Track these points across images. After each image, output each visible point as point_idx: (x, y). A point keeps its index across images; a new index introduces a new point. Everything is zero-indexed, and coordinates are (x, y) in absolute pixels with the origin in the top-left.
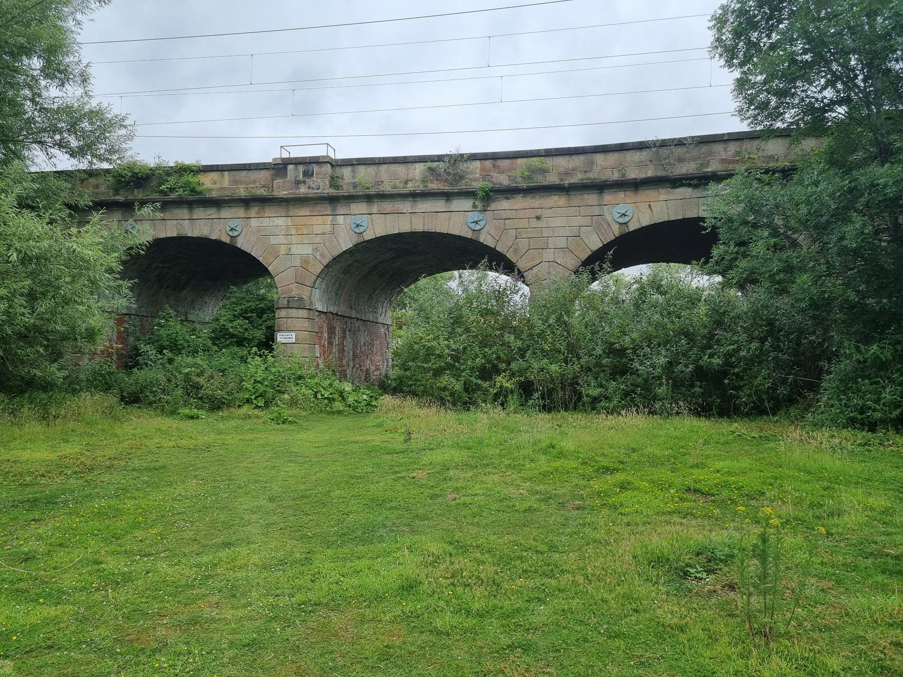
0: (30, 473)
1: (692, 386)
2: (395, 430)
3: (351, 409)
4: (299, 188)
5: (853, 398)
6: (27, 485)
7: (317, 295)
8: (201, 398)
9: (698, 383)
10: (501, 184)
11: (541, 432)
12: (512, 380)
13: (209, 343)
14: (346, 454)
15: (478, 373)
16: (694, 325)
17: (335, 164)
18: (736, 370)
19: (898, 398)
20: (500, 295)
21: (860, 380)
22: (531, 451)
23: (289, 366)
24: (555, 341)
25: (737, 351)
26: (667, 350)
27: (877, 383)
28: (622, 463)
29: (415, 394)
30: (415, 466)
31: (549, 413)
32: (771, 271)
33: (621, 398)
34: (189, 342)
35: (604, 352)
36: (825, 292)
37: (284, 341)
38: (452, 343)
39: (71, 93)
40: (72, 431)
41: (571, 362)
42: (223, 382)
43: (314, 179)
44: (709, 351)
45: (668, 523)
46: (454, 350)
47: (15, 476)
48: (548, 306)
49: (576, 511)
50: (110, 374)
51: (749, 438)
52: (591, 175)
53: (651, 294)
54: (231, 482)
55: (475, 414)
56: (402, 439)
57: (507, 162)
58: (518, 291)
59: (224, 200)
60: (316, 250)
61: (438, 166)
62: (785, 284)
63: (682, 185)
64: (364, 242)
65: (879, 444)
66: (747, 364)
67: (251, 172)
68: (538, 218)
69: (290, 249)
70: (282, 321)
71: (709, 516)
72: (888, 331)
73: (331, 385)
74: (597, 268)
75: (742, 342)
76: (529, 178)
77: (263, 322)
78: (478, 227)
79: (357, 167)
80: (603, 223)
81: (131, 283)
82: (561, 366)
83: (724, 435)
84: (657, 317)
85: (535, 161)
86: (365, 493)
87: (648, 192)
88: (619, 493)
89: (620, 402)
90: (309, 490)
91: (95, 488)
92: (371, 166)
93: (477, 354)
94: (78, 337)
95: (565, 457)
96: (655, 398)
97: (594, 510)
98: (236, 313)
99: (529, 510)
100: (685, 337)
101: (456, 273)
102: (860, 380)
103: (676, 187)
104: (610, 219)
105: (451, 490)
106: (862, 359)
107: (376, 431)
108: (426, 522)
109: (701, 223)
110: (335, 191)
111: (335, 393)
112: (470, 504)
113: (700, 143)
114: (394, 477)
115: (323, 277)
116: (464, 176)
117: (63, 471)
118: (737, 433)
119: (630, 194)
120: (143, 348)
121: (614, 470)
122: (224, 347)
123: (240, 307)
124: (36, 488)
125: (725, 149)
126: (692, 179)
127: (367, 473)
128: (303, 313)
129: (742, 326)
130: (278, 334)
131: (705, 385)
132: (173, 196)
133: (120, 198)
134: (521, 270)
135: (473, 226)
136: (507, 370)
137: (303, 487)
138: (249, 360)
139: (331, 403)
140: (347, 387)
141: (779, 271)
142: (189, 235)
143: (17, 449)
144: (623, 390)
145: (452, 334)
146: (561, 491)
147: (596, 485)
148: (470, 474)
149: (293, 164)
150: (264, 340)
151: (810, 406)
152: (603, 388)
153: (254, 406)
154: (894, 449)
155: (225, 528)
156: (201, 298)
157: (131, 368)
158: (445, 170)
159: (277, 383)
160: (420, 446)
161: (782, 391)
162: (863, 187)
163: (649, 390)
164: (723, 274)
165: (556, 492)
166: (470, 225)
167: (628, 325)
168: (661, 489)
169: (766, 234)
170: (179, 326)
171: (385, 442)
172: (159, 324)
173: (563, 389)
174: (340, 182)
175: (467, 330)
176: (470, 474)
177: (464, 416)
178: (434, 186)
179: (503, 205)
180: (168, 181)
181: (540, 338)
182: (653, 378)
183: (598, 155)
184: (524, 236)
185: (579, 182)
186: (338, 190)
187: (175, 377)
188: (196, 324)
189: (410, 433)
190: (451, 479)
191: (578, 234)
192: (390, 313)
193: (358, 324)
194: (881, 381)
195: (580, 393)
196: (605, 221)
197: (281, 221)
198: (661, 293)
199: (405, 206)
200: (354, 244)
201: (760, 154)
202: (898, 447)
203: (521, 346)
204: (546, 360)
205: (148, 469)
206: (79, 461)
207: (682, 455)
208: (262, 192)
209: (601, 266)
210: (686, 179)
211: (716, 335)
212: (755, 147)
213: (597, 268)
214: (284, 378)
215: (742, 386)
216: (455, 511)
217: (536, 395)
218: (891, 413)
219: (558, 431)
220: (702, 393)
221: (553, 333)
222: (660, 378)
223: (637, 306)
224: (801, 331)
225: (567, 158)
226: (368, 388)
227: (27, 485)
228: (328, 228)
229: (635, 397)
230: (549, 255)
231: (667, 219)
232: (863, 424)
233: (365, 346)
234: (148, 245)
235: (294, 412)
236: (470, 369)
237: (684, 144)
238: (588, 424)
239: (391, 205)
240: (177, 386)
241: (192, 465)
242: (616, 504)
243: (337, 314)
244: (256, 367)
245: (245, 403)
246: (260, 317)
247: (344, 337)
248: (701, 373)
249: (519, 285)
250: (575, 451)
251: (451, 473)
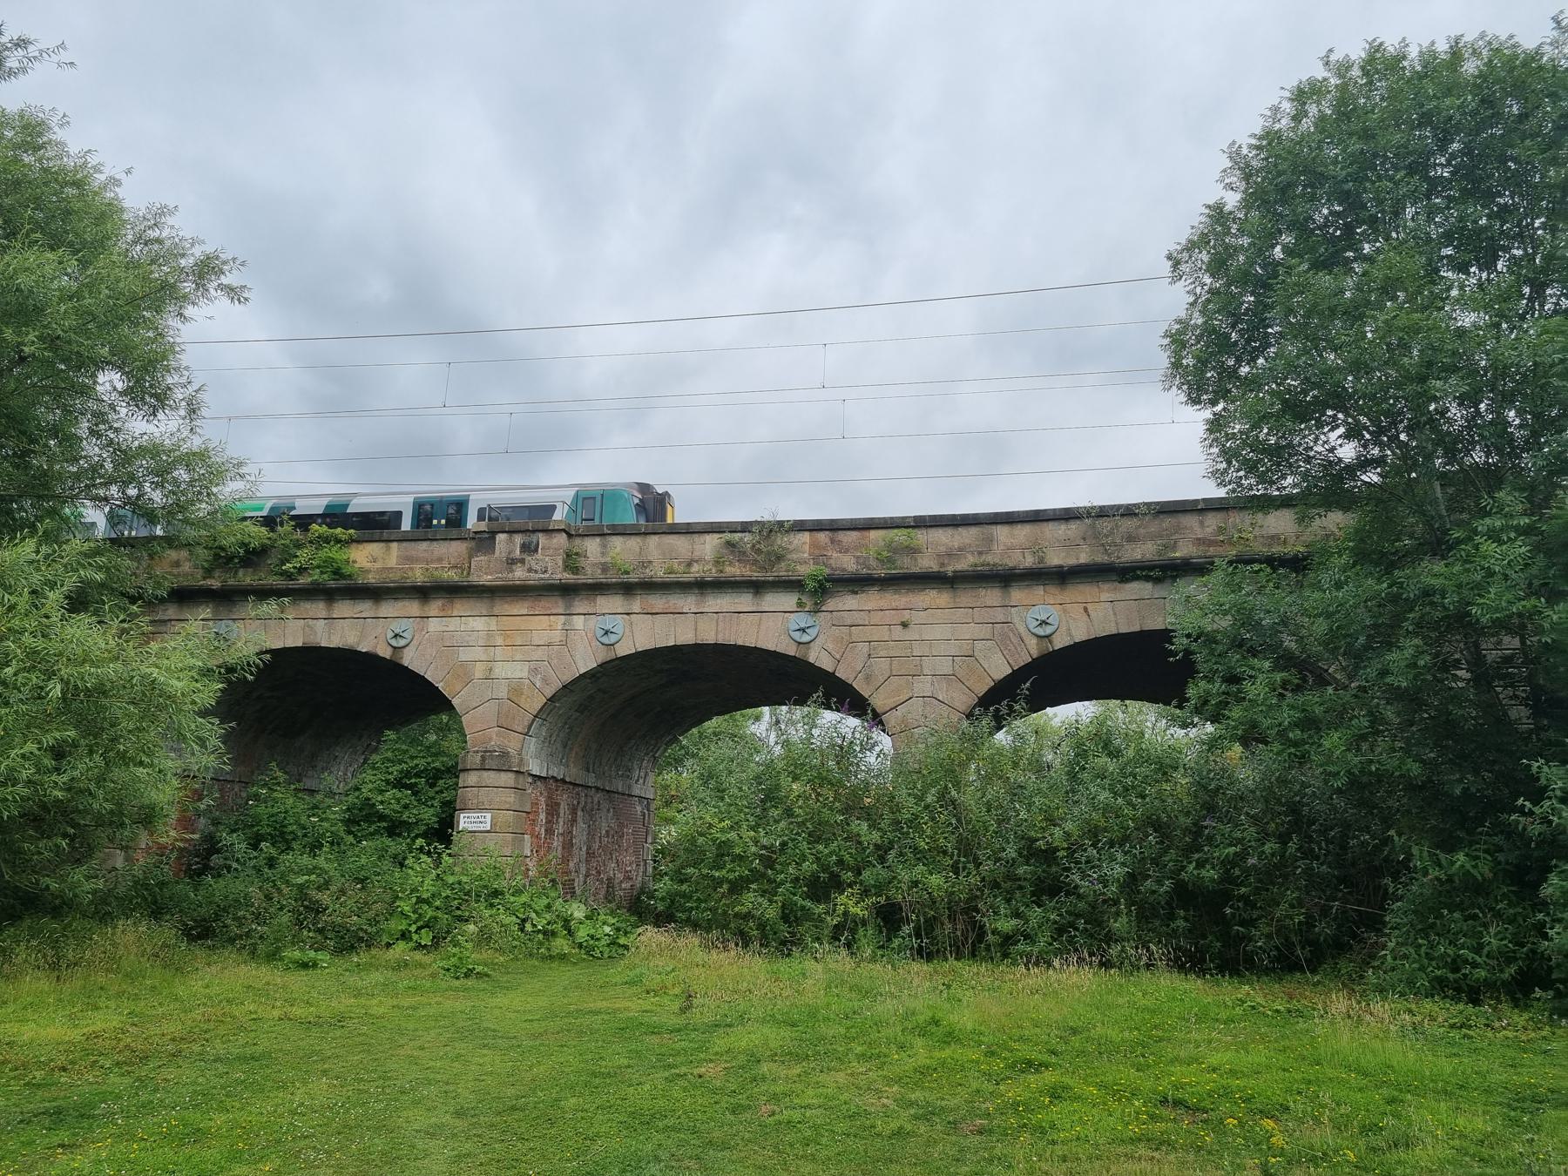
0: (40, 1065)
1: (1172, 917)
2: (662, 990)
3: (583, 952)
4: (512, 571)
6: (38, 1086)
8: (321, 931)
9: (1182, 913)
10: (844, 570)
12: (864, 901)
13: (341, 828)
14: (581, 1033)
15: (805, 889)
16: (1169, 809)
19: (1510, 945)
20: (844, 753)
21: (1446, 912)
22: (899, 1029)
23: (478, 873)
24: (936, 833)
25: (1242, 856)
26: (1126, 853)
27: (1475, 917)
28: (1054, 1053)
29: (695, 926)
30: (702, 1056)
31: (928, 962)
32: (1280, 725)
33: (1052, 937)
34: (304, 828)
35: (1020, 854)
36: (1371, 761)
38: (762, 834)
40: (101, 988)
42: (361, 901)
43: (539, 555)
44: (1196, 856)
45: (1129, 1157)
46: (764, 847)
47: (16, 1070)
48: (925, 772)
49: (978, 1137)
50: (162, 884)
51: (1269, 1013)
52: (989, 559)
53: (1094, 755)
55: (800, 963)
56: (676, 1006)
57: (854, 534)
58: (873, 746)
59: (388, 588)
60: (535, 671)
61: (741, 539)
62: (1307, 747)
63: (1137, 578)
66: (1260, 881)
67: (435, 543)
68: (905, 625)
69: (491, 670)
70: (470, 793)
71: (1198, 1146)
72: (1481, 829)
73: (548, 907)
74: (1004, 711)
75: (1249, 841)
76: (890, 560)
77: (437, 793)
78: (806, 638)
81: (224, 729)
82: (947, 877)
83: (1226, 1006)
84: (1104, 796)
85: (899, 536)
87: (1081, 587)
88: (1048, 1106)
89: (1051, 944)
90: (523, 1097)
91: (156, 1090)
92: (633, 537)
94: (127, 821)
96: (1110, 938)
97: (1007, 1135)
98: (390, 777)
99: (899, 1133)
100: (1155, 831)
102: (1446, 912)
104: (1022, 629)
105: (765, 1098)
106: (1443, 877)
107: (630, 992)
108: (727, 1153)
109: (1167, 645)
110: (572, 576)
112: (799, 1122)
115: (544, 717)
118: (1249, 1003)
120: (226, 838)
121: (1040, 1065)
122: (365, 837)
123: (398, 767)
124: (54, 1092)
125: (1202, 523)
126: (1152, 568)
127: (620, 1067)
128: (507, 779)
129: (1247, 814)
131: (1194, 916)
132: (304, 580)
133: (215, 583)
135: (797, 636)
136: (855, 883)
137: (511, 1091)
138: (410, 862)
139: (548, 940)
143: (11, 1022)
144: (1055, 922)
146: (953, 1102)
147: (1012, 1091)
148: (797, 1070)
149: (506, 532)
150: (436, 826)
151: (1373, 956)
153: (411, 944)
154: (1510, 1034)
155: (386, 1163)
157: (200, 873)
158: (754, 546)
159: (456, 902)
161: (1324, 929)
162: (1412, 596)
163: (1100, 924)
164: (1215, 719)
165: (944, 1103)
166: (792, 634)
167: (1058, 808)
168: (1119, 1100)
169: (1267, 664)
170: (291, 801)
171: (646, 1011)
172: (256, 797)
174: (582, 562)
175: (789, 813)
176: (797, 1070)
177: (783, 965)
178: (734, 571)
179: (847, 603)
180: (297, 556)
182: (1105, 901)
183: (999, 527)
184: (882, 653)
185: (970, 569)
186: (577, 574)
187: (279, 891)
188: (319, 797)
189: (690, 996)
191: (970, 653)
192: (651, 777)
193: (598, 796)
194: (1481, 915)
195: (982, 927)
197: (479, 624)
198: (1110, 755)
199: (688, 602)
200: (600, 662)
201: (1257, 532)
202: (1517, 1031)
203: (879, 842)
204: (921, 867)
205: (242, 1059)
206: (122, 1044)
207: (1156, 1041)
208: (451, 576)
209: (1010, 707)
210: (1142, 568)
211: (1206, 828)
212: (1248, 522)
213: (1004, 711)
214: (468, 893)
215: (1256, 920)
216: (774, 1134)
217: (906, 929)
218: (1502, 971)
221: (933, 819)
222: (1116, 902)
223: (1072, 776)
224: (1346, 826)
225: (950, 531)
226: (612, 913)
227: (38, 1086)
228: (557, 636)
230: (923, 686)
232: (1458, 990)
233: (608, 836)
235: (485, 955)
236: (791, 882)
237: (1136, 515)
238: (997, 983)
239: (664, 600)
242: (1044, 1124)
243: (563, 781)
244: (421, 874)
245: (397, 939)
247: (574, 821)
248: (1184, 894)
249: (874, 735)
250: (973, 1032)
251: (765, 1068)
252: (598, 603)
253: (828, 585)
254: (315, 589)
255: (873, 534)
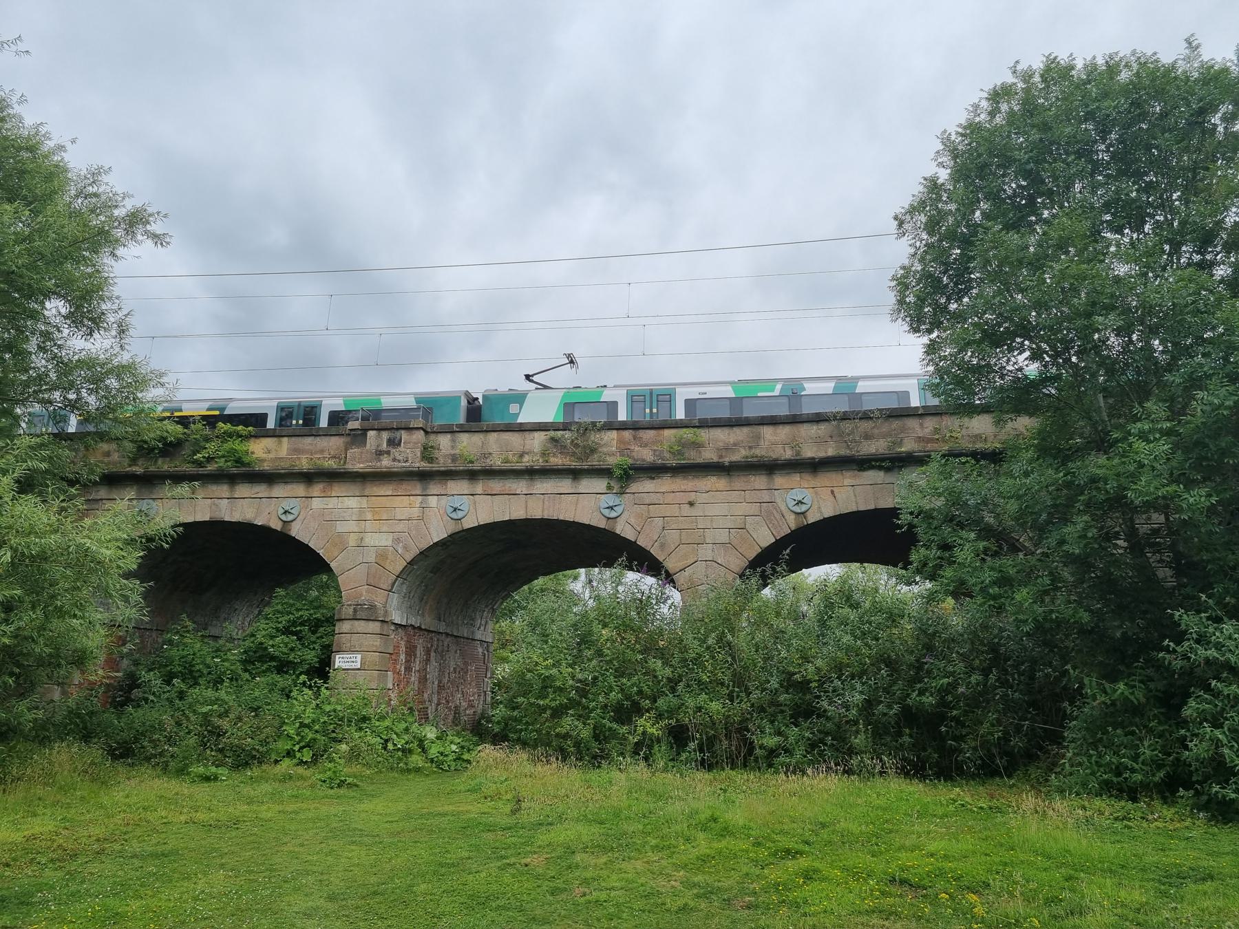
1: (900, 734)
2: (496, 797)
5: (1105, 753)
7: (395, 602)
8: (221, 751)
10: (644, 460)
11: (699, 800)
12: (658, 723)
13: (239, 667)
15: (612, 714)
17: (429, 430)
18: (955, 712)
19: (1160, 755)
20: (643, 604)
22: (685, 825)
23: (350, 702)
24: (716, 669)
25: (953, 686)
26: (863, 684)
27: (1133, 733)
28: (807, 843)
29: (524, 744)
30: (528, 849)
31: (709, 771)
32: (982, 582)
33: (806, 751)
35: (782, 686)
36: (1052, 611)
37: (345, 666)
38: (578, 671)
39: (99, 345)
40: (40, 799)
41: (737, 698)
42: (255, 726)
43: (402, 448)
44: (918, 686)
46: (580, 681)
48: (706, 620)
49: (747, 911)
50: (91, 714)
51: (975, 809)
52: (758, 452)
53: (839, 607)
54: (274, 874)
56: (508, 809)
57: (652, 433)
59: (280, 474)
60: (398, 540)
61: (563, 436)
63: (872, 468)
64: (463, 531)
65: (1141, 818)
66: (967, 705)
67: (318, 438)
68: (691, 504)
70: (344, 638)
73: (407, 730)
74: (769, 572)
75: (959, 674)
76: (680, 453)
77: (318, 638)
78: (613, 514)
79: (457, 435)
80: (775, 512)
83: (942, 805)
84: (847, 639)
86: (461, 887)
87: (828, 474)
88: (802, 886)
89: (805, 756)
91: (83, 882)
92: (476, 434)
93: (611, 687)
94: (63, 662)
95: (732, 834)
96: (851, 752)
99: (684, 909)
101: (582, 571)
102: (1110, 729)
103: (865, 470)
104: (783, 508)
105: (577, 882)
106: (1109, 702)
111: (412, 742)
112: (605, 901)
113: (890, 416)
114: (499, 864)
115: (404, 577)
116: (596, 449)
117: (35, 858)
118: (959, 802)
119: (807, 476)
120: (145, 676)
121: (796, 853)
122: (258, 674)
123: (286, 618)
125: (921, 425)
126: (883, 460)
128: (374, 627)
129: (958, 652)
130: (337, 656)
131: (917, 733)
132: (211, 467)
133: (138, 470)
134: (670, 572)
135: (606, 512)
136: (652, 708)
137: (373, 879)
139: (406, 757)
140: (430, 733)
141: (994, 583)
142: (227, 519)
144: (809, 739)
145: (577, 660)
146: (726, 884)
147: (773, 874)
148: (604, 859)
150: (317, 665)
152: (782, 736)
153: (295, 761)
156: (229, 603)
158: (573, 441)
159: (332, 726)
160: (534, 818)
161: (1017, 742)
162: (1082, 482)
164: (932, 578)
165: (720, 884)
168: (858, 880)
171: (485, 813)
172: (170, 642)
173: (728, 736)
174: (436, 454)
175: (599, 653)
176: (604, 859)
177: (594, 775)
178: (557, 461)
179: (645, 487)
180: (206, 448)
181: (696, 665)
182: (847, 722)
183: (765, 427)
184: (673, 527)
185: (743, 460)
186: (431, 463)
187: (188, 718)
188: (221, 642)
189: (519, 801)
190: (577, 866)
192: (491, 625)
194: (1137, 731)
196: (777, 509)
197: (352, 503)
199: (520, 486)
200: (449, 533)
201: (964, 432)
203: (671, 676)
204: (704, 696)
205: (154, 855)
208: (331, 464)
209: (774, 570)
210: (876, 460)
213: (769, 572)
214: (341, 719)
215: (965, 736)
216: (585, 911)
217: (692, 745)
218: (1153, 775)
219: (722, 798)
220: (913, 745)
222: (856, 723)
223: (823, 623)
224: (1034, 662)
225: (726, 431)
226: (458, 734)
228: (416, 512)
229: (825, 750)
230: (706, 552)
231: (854, 509)
232: (1121, 791)
234: (175, 536)
235: (355, 770)
236: (601, 708)
237: (871, 418)
239: (501, 484)
240: (189, 733)
241: (216, 850)
242: (798, 900)
243: (420, 628)
244: (304, 704)
245: (284, 757)
246: (314, 632)
247: (428, 660)
248: (909, 716)
250: (744, 827)
251: (578, 858)
252: (449, 486)
253: (631, 472)
254: (219, 475)
255: (667, 432)
